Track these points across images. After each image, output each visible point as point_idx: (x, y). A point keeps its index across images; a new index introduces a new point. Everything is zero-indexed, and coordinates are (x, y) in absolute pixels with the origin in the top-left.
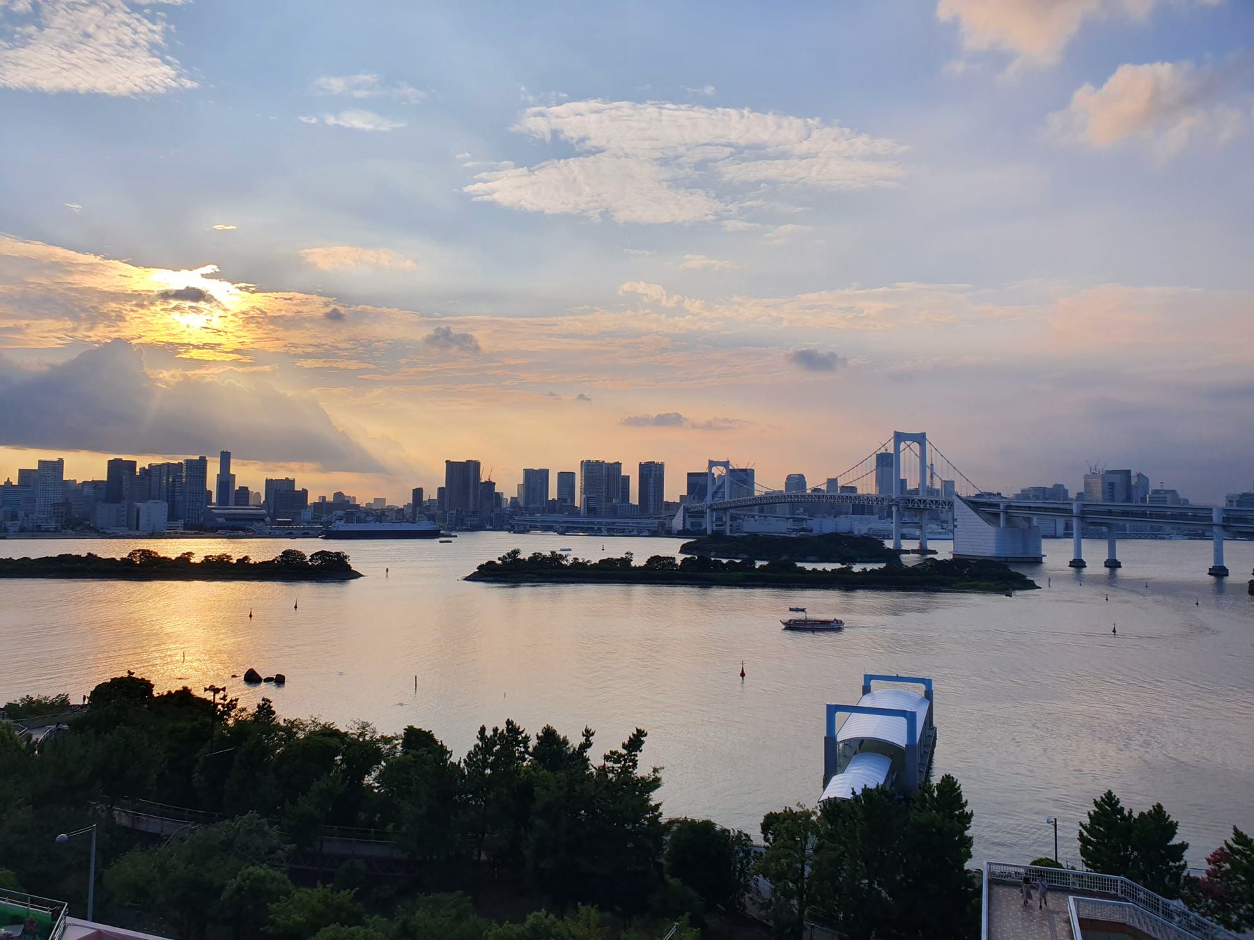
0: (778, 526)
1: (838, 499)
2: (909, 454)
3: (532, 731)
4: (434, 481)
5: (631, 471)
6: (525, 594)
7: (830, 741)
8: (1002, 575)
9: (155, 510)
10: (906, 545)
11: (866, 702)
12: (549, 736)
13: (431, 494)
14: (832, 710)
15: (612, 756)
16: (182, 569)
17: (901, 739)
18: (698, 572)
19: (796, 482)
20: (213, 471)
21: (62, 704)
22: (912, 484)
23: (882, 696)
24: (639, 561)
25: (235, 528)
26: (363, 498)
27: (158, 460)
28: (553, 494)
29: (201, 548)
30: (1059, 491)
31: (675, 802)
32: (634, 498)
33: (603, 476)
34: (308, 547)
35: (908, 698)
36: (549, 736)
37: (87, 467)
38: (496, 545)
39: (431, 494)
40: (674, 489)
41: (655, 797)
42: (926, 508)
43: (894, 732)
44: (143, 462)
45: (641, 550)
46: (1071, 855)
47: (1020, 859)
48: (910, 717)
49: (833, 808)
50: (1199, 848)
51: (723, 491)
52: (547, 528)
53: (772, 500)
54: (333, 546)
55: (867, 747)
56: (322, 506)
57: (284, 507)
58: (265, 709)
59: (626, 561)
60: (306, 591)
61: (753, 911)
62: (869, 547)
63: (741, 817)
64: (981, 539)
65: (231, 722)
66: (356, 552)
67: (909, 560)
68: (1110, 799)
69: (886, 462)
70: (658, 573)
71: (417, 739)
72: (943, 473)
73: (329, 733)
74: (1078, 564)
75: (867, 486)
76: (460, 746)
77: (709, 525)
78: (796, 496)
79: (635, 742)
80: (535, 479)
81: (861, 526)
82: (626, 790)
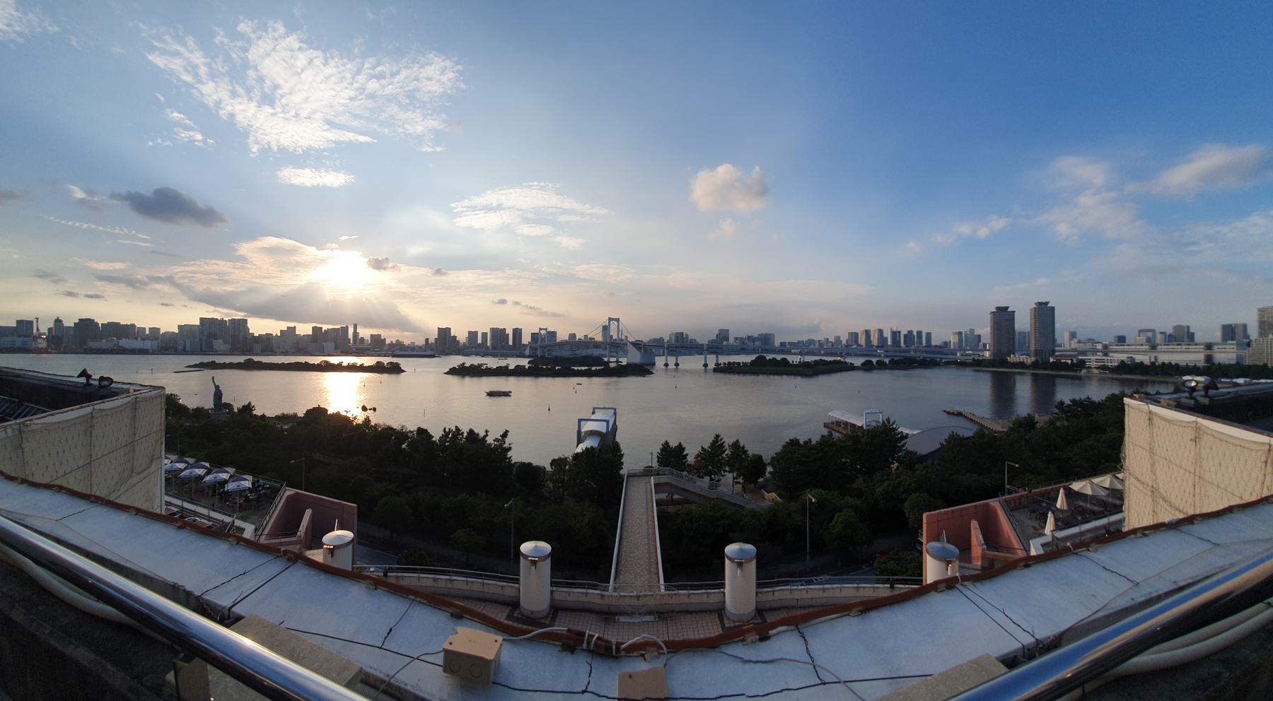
0: (566, 353)
1: (589, 343)
2: (614, 325)
3: (465, 430)
4: (433, 336)
5: (510, 332)
6: (468, 380)
7: (579, 432)
8: (642, 370)
9: (329, 346)
10: (612, 359)
11: (593, 417)
12: (471, 432)
13: (432, 340)
14: (580, 421)
15: (496, 440)
16: (339, 368)
17: (604, 431)
18: (535, 371)
19: (573, 336)
20: (351, 331)
21: (295, 416)
22: (615, 337)
23: (599, 415)
24: (512, 367)
25: (359, 352)
26: (407, 342)
27: (331, 327)
28: (479, 341)
29: (347, 360)
30: (661, 339)
31: (516, 456)
32: (511, 343)
33: (499, 334)
34: (386, 360)
35: (607, 415)
36: (471, 432)
37: (304, 329)
38: (456, 361)
39: (432, 340)
40: (526, 339)
41: (509, 454)
42: (617, 346)
43: (601, 427)
44: (325, 327)
45: (512, 363)
46: (655, 465)
47: (639, 467)
48: (607, 422)
49: (576, 456)
50: (691, 453)
51: (544, 340)
52: (477, 355)
53: (563, 343)
54: (395, 360)
55: (592, 433)
56: (391, 344)
57: (377, 346)
58: (367, 420)
59: (507, 367)
60: (385, 376)
61: (546, 494)
62: (598, 360)
63: (543, 460)
64: (634, 357)
65: (247, 484)
66: (403, 362)
67: (612, 365)
68: (667, 443)
69: (606, 328)
70: (519, 372)
71: (422, 432)
72: (625, 334)
73: (390, 428)
74: (666, 365)
75: (599, 338)
76: (437, 435)
77: (539, 353)
78: (572, 342)
79: (505, 435)
80: (473, 335)
81: (596, 352)
82: (501, 450)
